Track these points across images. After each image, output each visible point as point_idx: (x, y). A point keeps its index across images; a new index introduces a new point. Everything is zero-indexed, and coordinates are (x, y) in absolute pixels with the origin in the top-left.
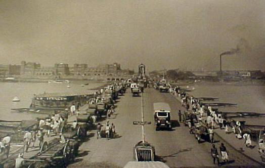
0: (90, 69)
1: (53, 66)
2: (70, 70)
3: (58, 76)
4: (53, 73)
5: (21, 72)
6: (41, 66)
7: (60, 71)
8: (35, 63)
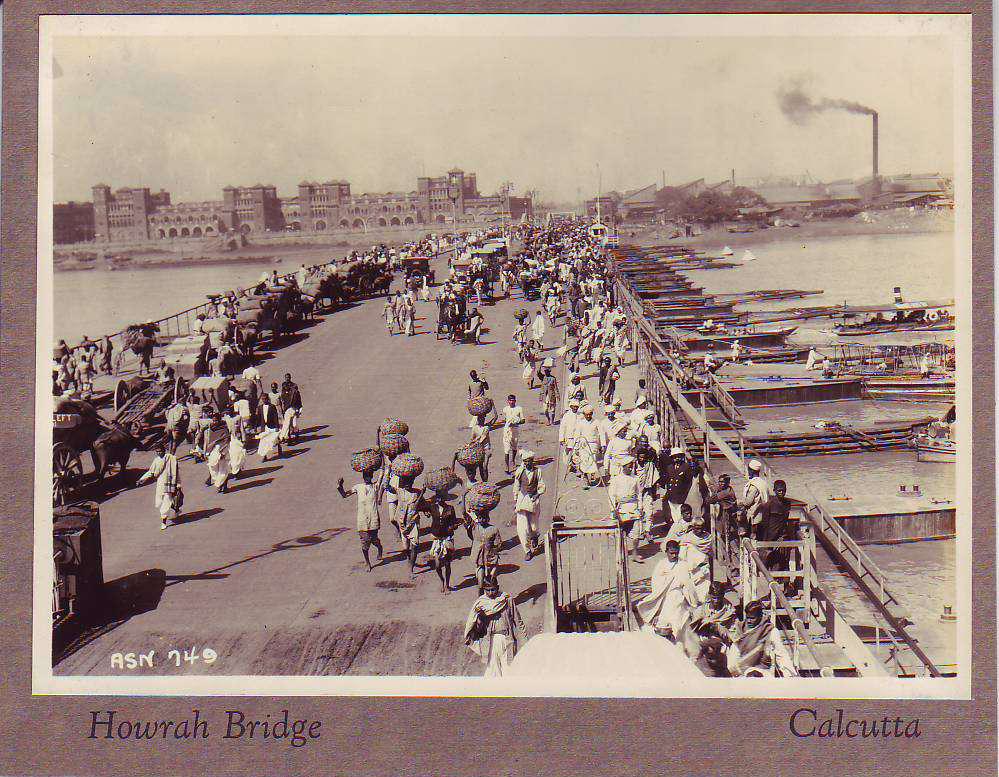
0: (359, 202)
1: (218, 196)
2: (286, 209)
3: (237, 237)
4: (222, 228)
5: (100, 230)
6: (174, 200)
7: (250, 217)
8: (147, 191)
